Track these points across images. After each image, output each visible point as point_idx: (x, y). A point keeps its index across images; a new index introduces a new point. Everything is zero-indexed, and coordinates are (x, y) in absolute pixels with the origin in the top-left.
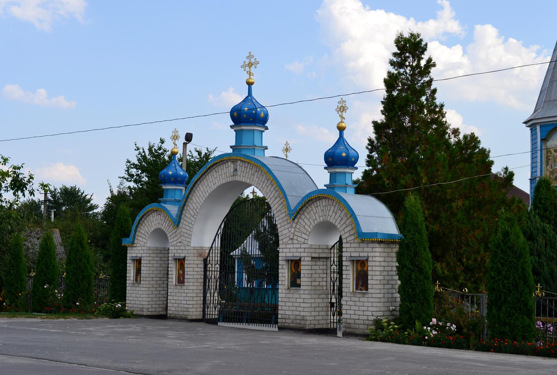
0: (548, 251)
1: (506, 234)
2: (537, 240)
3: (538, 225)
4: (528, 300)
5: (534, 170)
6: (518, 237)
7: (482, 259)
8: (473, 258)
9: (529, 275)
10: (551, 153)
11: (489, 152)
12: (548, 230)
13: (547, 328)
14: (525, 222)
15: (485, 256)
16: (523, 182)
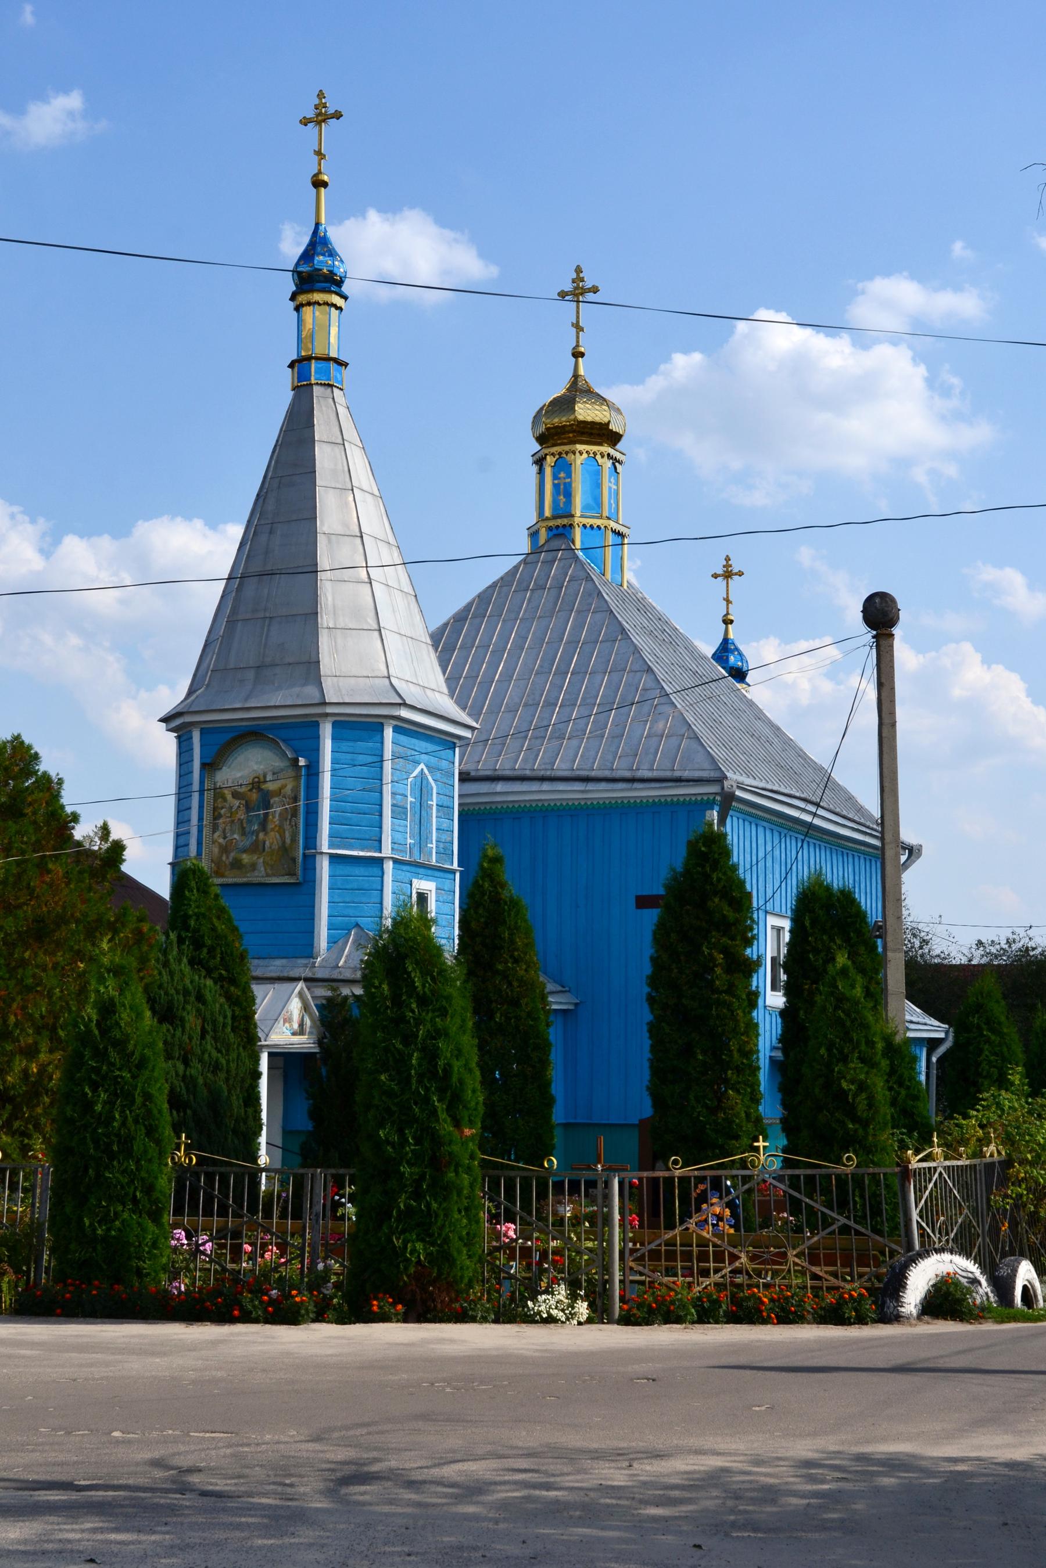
0: (209, 1047)
1: (107, 1009)
2: (182, 1020)
3: (187, 982)
4: (156, 1178)
5: (182, 841)
6: (139, 1015)
7: (42, 1069)
8: (17, 1069)
9: (160, 1112)
10: (225, 800)
11: (60, 782)
12: (209, 997)
13: (198, 1245)
14: (156, 972)
15: (49, 1064)
16: (150, 866)
